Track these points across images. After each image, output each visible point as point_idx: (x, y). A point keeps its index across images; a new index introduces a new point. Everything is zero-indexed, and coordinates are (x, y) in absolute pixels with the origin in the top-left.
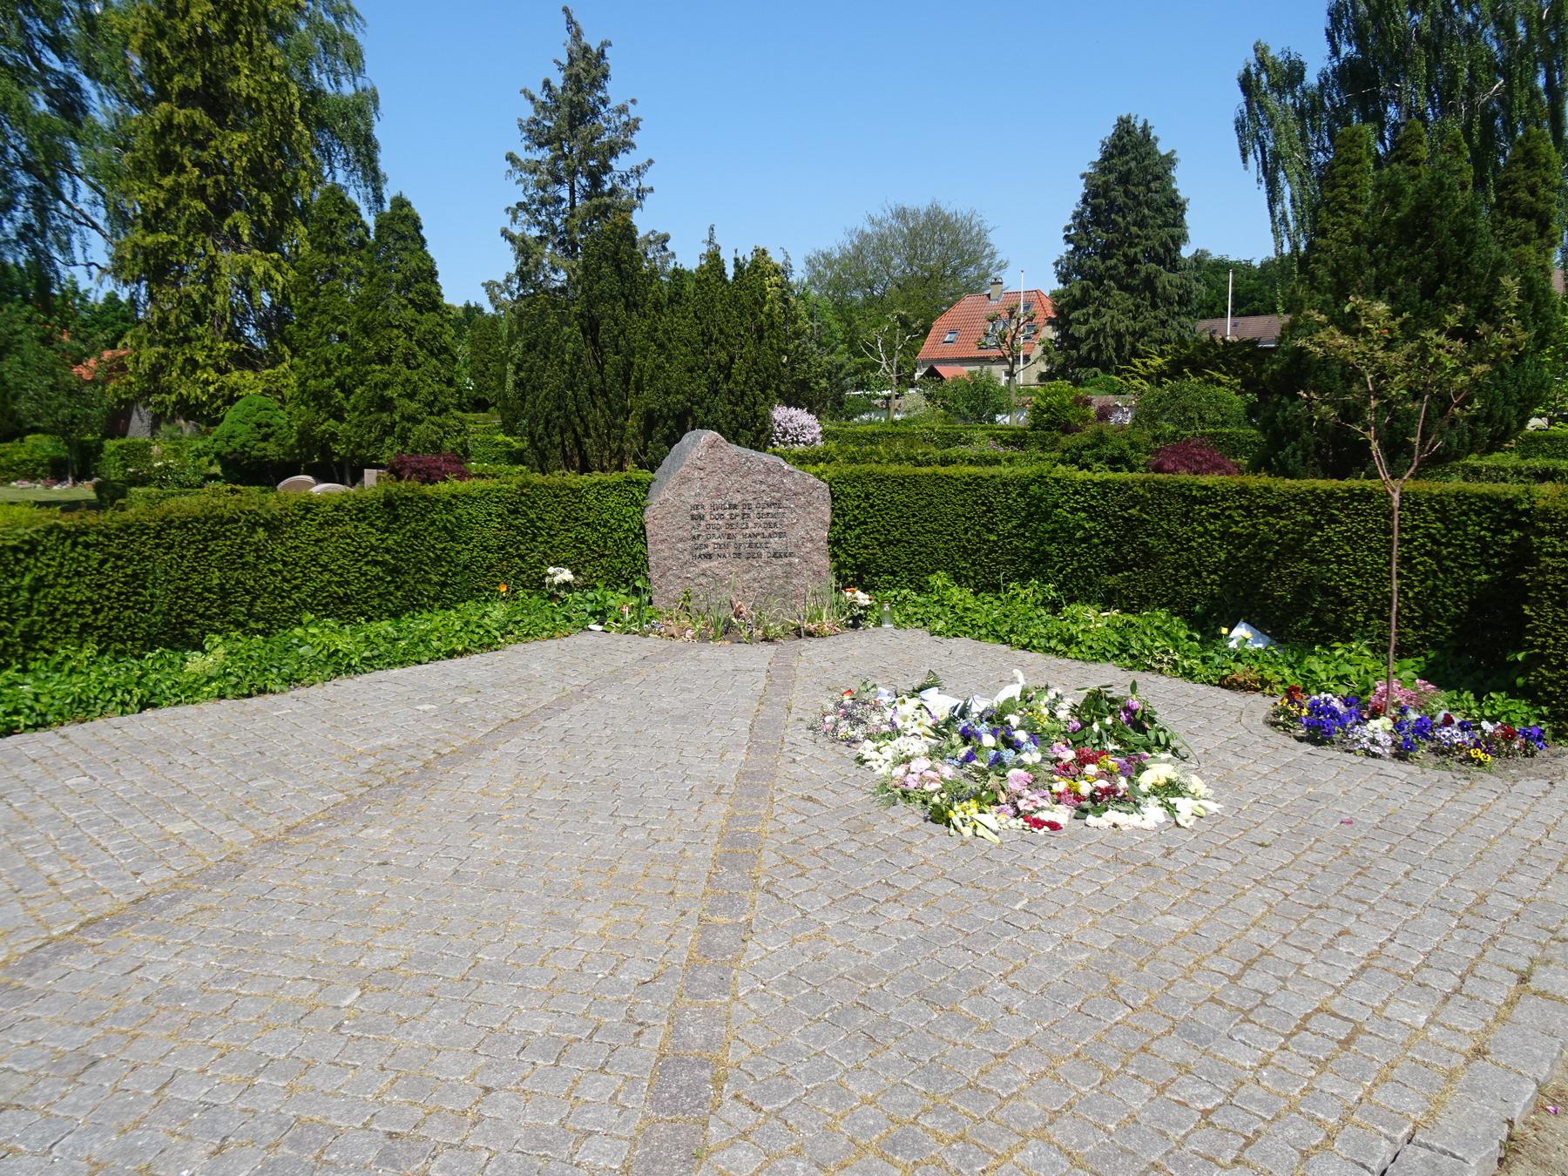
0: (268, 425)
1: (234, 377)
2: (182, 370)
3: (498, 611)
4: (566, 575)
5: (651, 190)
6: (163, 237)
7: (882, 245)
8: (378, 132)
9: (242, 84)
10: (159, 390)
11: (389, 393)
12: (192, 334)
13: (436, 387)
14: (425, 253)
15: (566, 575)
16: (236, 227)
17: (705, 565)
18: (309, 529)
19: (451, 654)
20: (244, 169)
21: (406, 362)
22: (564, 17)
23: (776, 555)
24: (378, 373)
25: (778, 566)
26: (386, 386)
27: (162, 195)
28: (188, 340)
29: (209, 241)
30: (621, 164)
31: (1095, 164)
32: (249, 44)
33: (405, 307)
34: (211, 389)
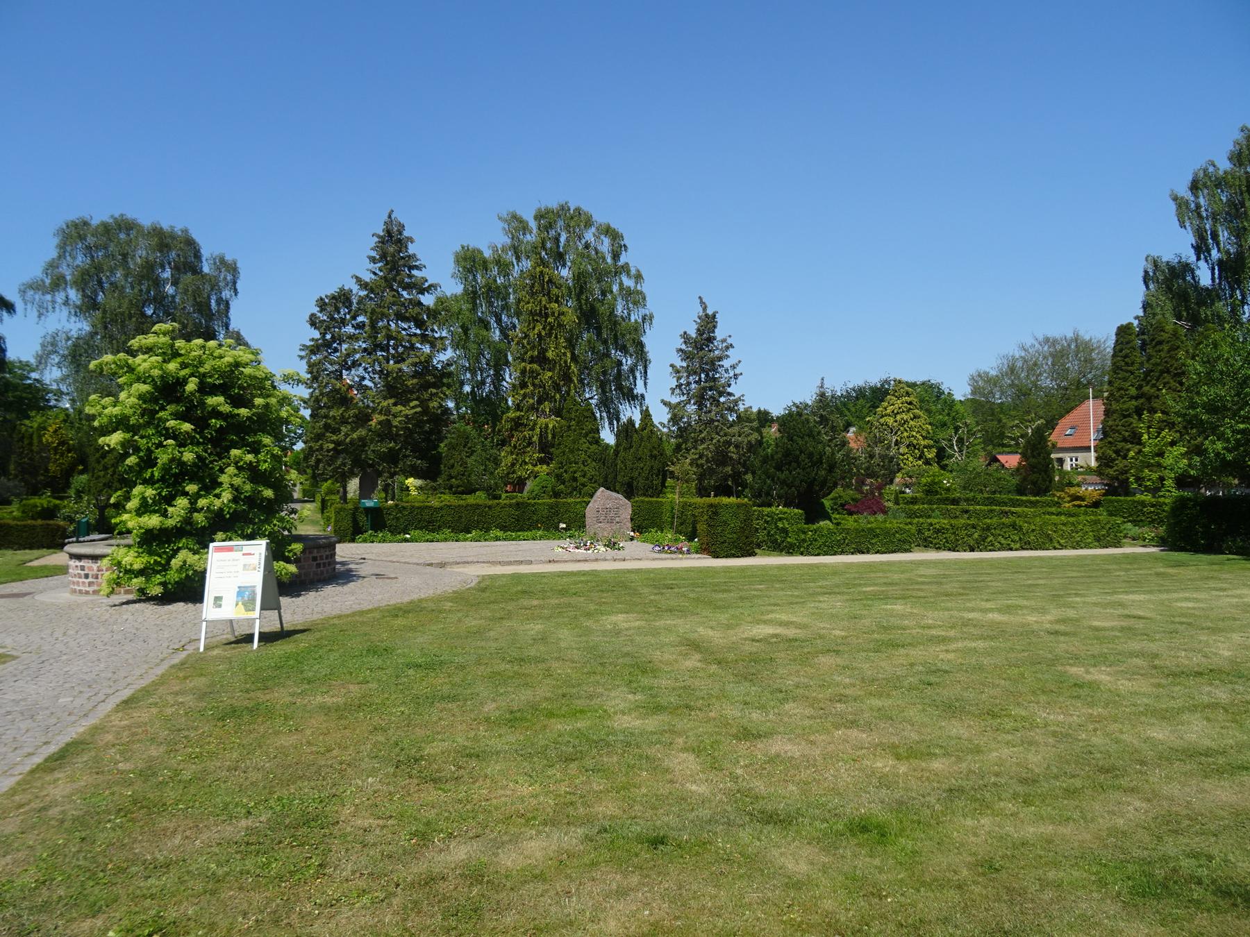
2: (521, 465)
3: (540, 532)
4: (564, 526)
13: (593, 473)
15: (564, 526)
21: (583, 464)
28: (524, 452)
30: (726, 363)
32: (556, 337)
33: (585, 443)
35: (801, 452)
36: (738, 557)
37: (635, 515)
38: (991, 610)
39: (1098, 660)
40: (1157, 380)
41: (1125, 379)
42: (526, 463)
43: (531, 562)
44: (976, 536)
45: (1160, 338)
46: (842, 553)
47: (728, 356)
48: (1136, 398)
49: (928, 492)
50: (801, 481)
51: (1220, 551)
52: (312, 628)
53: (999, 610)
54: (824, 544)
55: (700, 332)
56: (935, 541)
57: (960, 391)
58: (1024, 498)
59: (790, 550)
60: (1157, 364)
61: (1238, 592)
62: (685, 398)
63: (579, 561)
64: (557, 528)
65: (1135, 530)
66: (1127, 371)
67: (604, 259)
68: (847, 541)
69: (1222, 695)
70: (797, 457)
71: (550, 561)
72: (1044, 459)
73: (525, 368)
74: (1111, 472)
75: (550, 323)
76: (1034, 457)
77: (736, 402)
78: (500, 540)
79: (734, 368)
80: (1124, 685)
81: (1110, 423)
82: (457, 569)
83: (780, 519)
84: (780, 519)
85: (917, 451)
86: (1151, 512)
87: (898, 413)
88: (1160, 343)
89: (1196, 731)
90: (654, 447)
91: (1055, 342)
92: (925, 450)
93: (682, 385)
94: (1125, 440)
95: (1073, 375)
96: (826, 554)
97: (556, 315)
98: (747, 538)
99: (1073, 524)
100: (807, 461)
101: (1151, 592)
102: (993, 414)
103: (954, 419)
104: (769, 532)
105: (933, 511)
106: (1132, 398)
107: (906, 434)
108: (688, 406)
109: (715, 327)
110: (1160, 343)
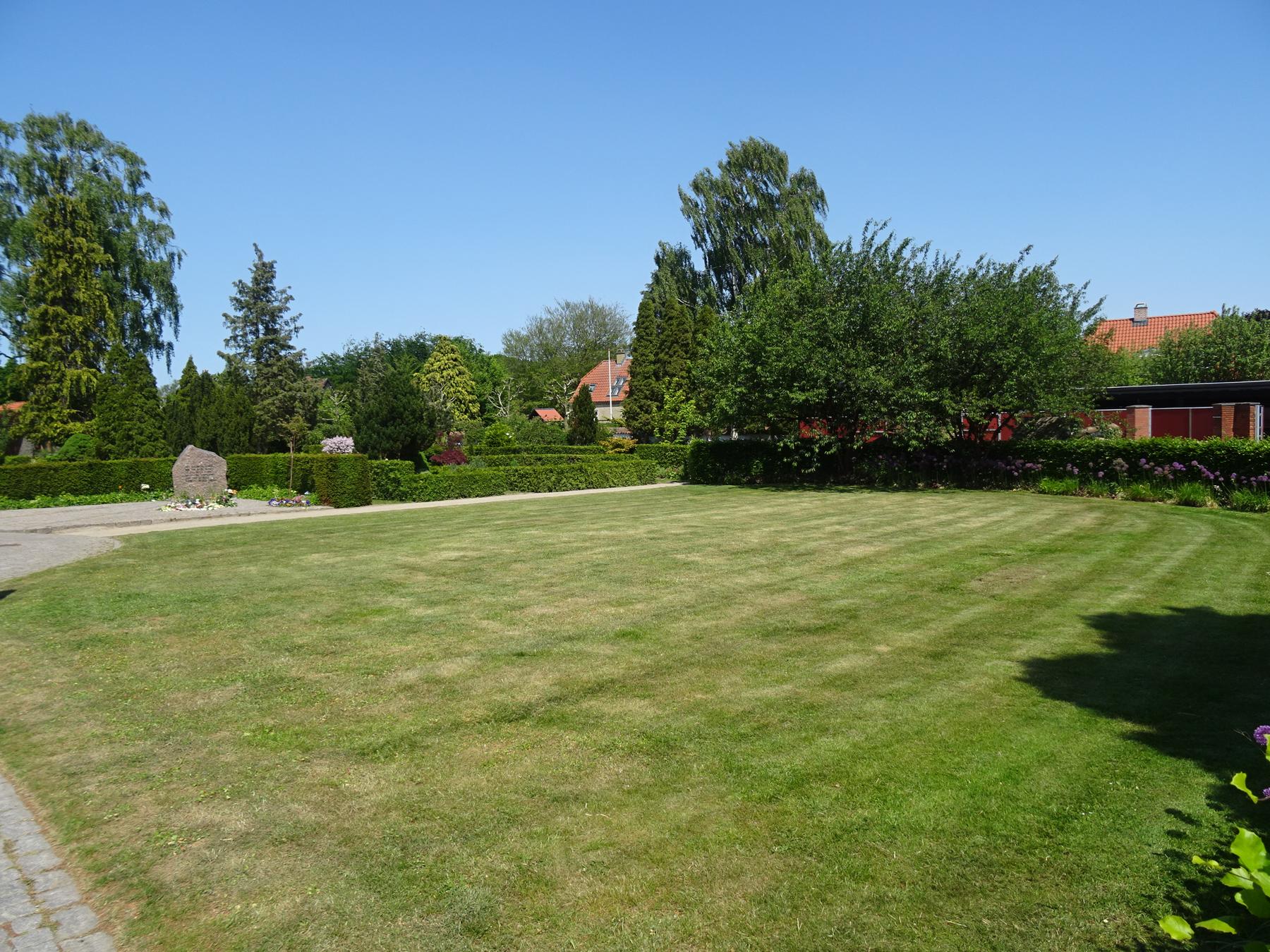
0: (85, 447)
1: (71, 425)
2: (46, 422)
4: (148, 486)
5: (302, 327)
6: (41, 364)
7: (558, 328)
8: (174, 282)
9: (81, 296)
10: (35, 431)
11: (131, 433)
12: (51, 406)
13: (153, 430)
14: (152, 375)
15: (148, 486)
16: (75, 357)
17: (190, 483)
18: (66, 470)
19: (103, 503)
20: (80, 333)
22: (254, 248)
23: (211, 480)
24: (128, 424)
25: (212, 484)
26: (130, 430)
27: (41, 345)
28: (50, 408)
29: (62, 365)
30: (286, 316)
31: (649, 286)
32: (85, 277)
33: (140, 398)
34: (58, 431)
35: (405, 409)
36: (357, 506)
37: (231, 472)
38: (601, 529)
39: (690, 550)
40: (670, 349)
41: (646, 347)
42: (52, 420)
43: (150, 522)
44: (553, 479)
45: (670, 315)
46: (449, 497)
47: (287, 309)
48: (654, 363)
49: (491, 444)
50: (406, 436)
51: (723, 483)
52: (15, 588)
53: (606, 529)
54: (433, 490)
55: (256, 281)
56: (520, 485)
57: (493, 346)
58: (575, 447)
59: (403, 498)
60: (668, 336)
61: (744, 508)
62: (242, 350)
63: (203, 518)
64: (138, 489)
65: (662, 471)
66: (647, 340)
67: (119, 186)
68: (452, 488)
69: (763, 561)
70: (402, 414)
71: (171, 520)
72: (590, 413)
73: (46, 312)
74: (636, 424)
75: (76, 261)
76: (581, 412)
77: (300, 355)
78: (73, 504)
79: (295, 321)
80: (711, 561)
81: (635, 383)
82: (66, 533)
83: (392, 470)
84: (392, 470)
85: (463, 406)
86: (671, 456)
87: (444, 369)
88: (671, 318)
89: (758, 578)
90: (239, 403)
91: (576, 307)
92: (470, 404)
93: (237, 336)
94: (646, 398)
95: (591, 338)
96: (435, 499)
97: (85, 251)
98: (365, 488)
99: (623, 467)
100: (411, 417)
101: (692, 512)
102: (524, 371)
103: (492, 375)
104: (379, 482)
105: (511, 460)
106: (651, 362)
107: (452, 389)
108: (246, 359)
109: (273, 277)
110: (671, 318)
